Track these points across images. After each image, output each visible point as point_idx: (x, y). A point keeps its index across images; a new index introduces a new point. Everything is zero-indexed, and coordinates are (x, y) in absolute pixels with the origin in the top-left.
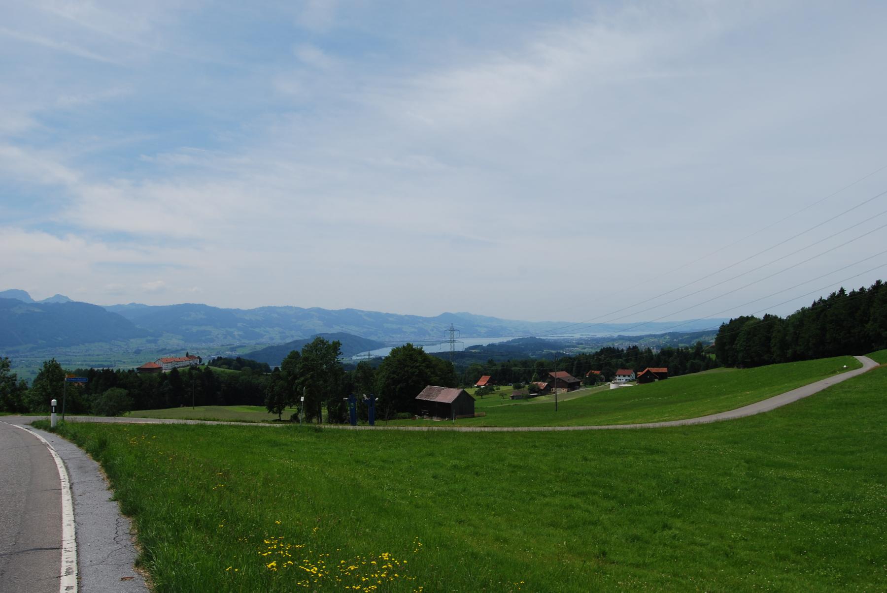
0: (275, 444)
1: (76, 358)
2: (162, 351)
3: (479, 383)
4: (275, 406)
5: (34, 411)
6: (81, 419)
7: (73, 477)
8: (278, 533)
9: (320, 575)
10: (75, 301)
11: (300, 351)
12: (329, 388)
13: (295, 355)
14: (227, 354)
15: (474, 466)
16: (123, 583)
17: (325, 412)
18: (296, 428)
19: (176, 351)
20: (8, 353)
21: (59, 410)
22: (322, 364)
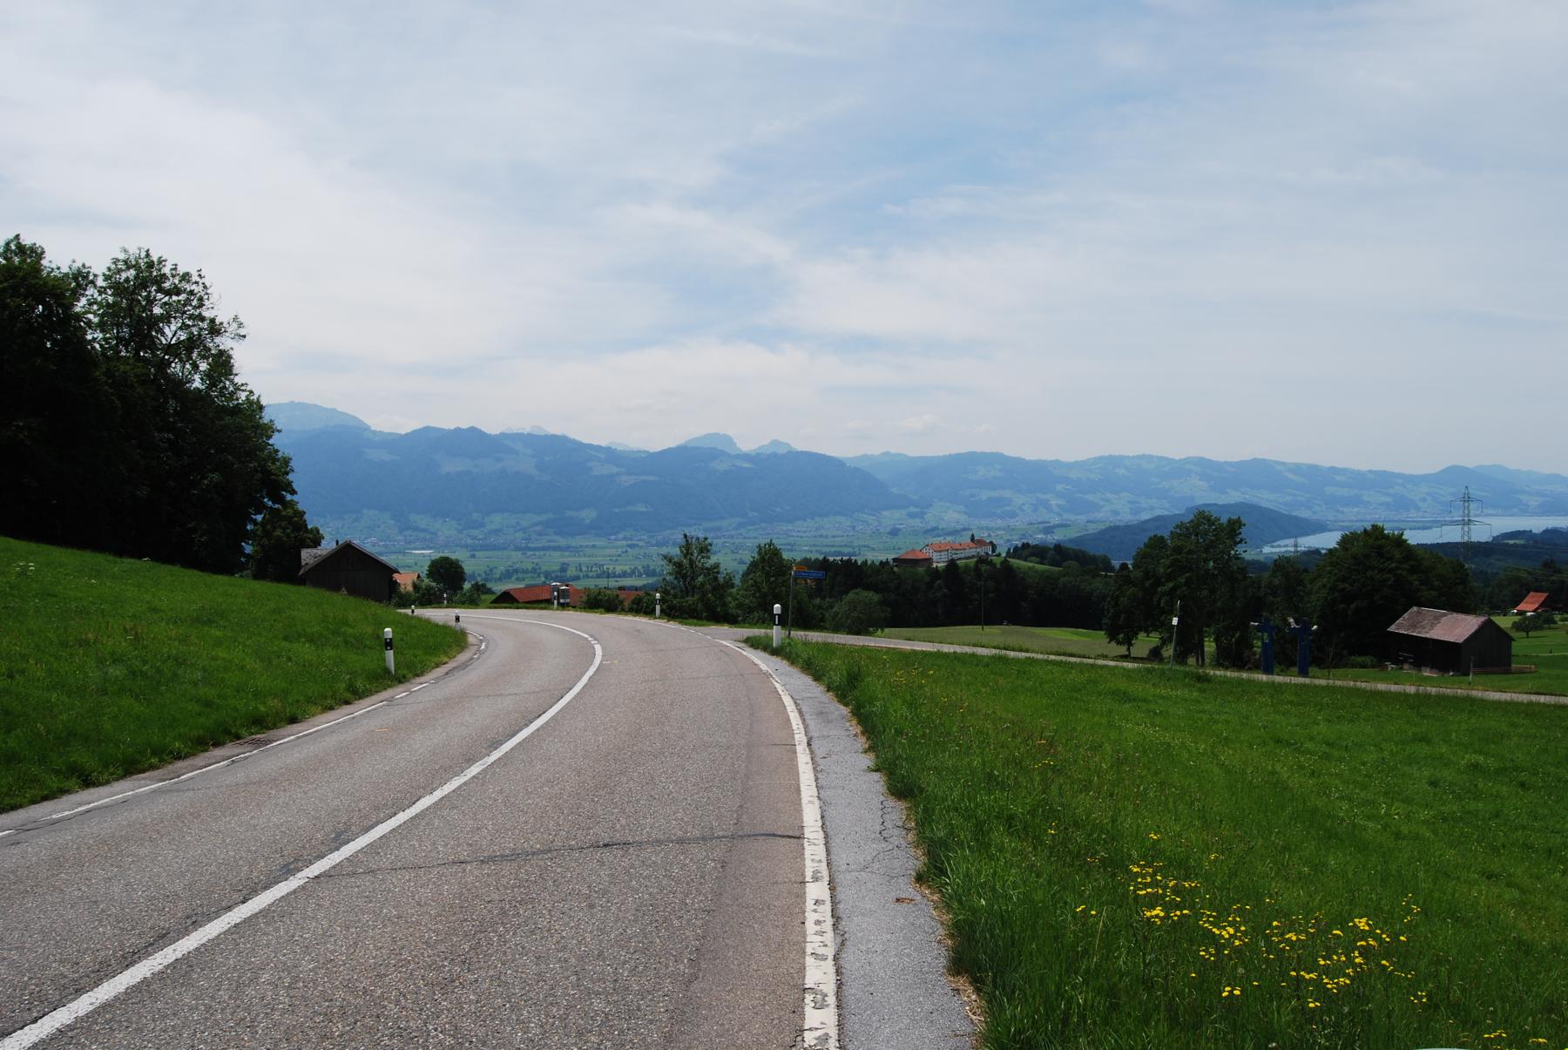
0: (1126, 697)
1: (803, 541)
2: (932, 531)
3: (1522, 607)
4: (1122, 631)
5: (744, 621)
6: (815, 636)
7: (811, 727)
8: (1151, 854)
9: (1237, 943)
10: (656, 446)
11: (1166, 535)
12: (1219, 604)
13: (1157, 543)
14: (1038, 538)
15: (1516, 769)
16: (899, 907)
17: (1210, 646)
18: (1163, 673)
19: (954, 532)
20: (706, 530)
21: (783, 622)
22: (1206, 561)
